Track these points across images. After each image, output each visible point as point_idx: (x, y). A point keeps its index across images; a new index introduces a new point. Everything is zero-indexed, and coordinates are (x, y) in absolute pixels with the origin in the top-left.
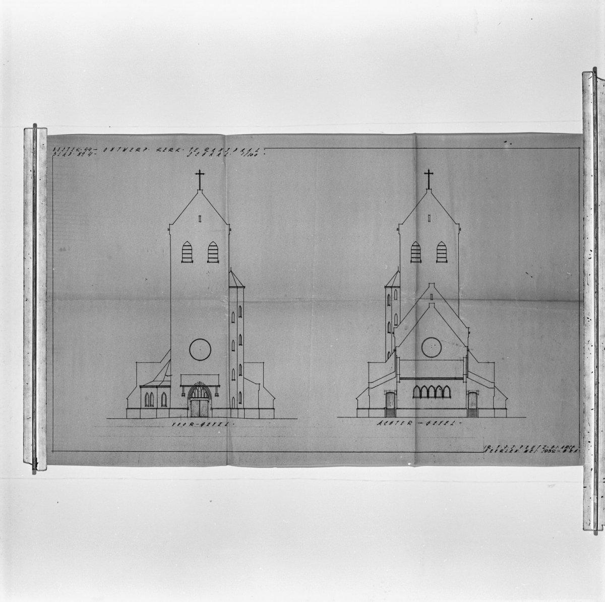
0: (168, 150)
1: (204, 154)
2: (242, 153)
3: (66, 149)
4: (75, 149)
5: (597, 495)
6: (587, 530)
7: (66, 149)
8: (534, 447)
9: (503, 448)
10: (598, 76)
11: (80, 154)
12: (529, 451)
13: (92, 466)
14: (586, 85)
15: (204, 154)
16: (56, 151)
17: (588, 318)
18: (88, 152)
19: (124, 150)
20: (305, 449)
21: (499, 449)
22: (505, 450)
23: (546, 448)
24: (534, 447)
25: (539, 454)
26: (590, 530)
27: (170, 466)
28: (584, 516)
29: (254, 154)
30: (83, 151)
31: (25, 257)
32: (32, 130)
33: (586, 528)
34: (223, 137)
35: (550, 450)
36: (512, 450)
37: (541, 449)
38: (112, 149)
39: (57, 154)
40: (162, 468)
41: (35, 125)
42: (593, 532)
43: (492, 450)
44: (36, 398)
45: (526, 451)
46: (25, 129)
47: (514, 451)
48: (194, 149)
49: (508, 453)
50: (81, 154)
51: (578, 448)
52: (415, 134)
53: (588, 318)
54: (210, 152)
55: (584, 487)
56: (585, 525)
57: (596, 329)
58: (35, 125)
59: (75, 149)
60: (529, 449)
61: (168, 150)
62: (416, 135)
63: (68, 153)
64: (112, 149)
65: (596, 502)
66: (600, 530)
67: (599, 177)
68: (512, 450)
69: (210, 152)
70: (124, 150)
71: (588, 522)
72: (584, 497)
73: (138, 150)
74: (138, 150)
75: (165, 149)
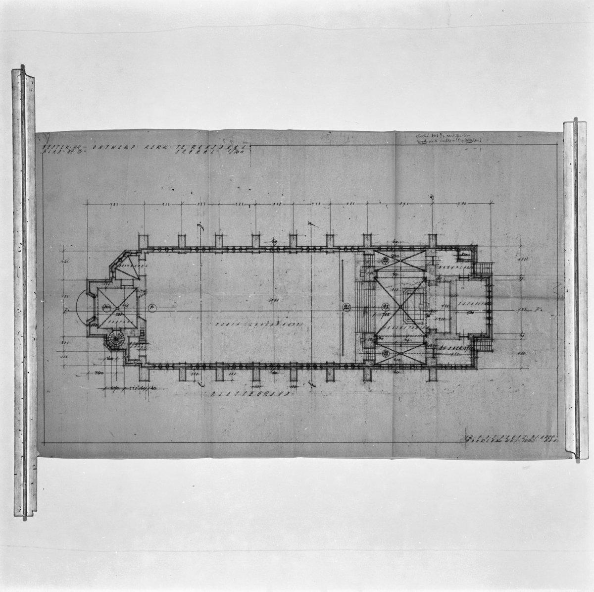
0: (155, 147)
1: (191, 151)
2: (228, 150)
8: (514, 436)
9: (484, 438)
10: (27, 73)
11: (69, 151)
13: (508, 460)
14: (15, 83)
15: (191, 151)
21: (480, 439)
22: (486, 440)
23: (526, 438)
27: (514, 460)
28: (14, 503)
29: (241, 150)
34: (209, 133)
37: (521, 439)
40: (551, 461)
42: (22, 518)
43: (473, 440)
44: (576, 394)
45: (507, 441)
46: (564, 123)
47: (480, 441)
48: (181, 147)
50: (70, 152)
51: (556, 438)
52: (395, 131)
54: (196, 149)
55: (15, 474)
56: (16, 511)
57: (576, 326)
60: (510, 438)
61: (155, 147)
62: (396, 133)
63: (58, 151)
70: (113, 148)
72: (15, 483)
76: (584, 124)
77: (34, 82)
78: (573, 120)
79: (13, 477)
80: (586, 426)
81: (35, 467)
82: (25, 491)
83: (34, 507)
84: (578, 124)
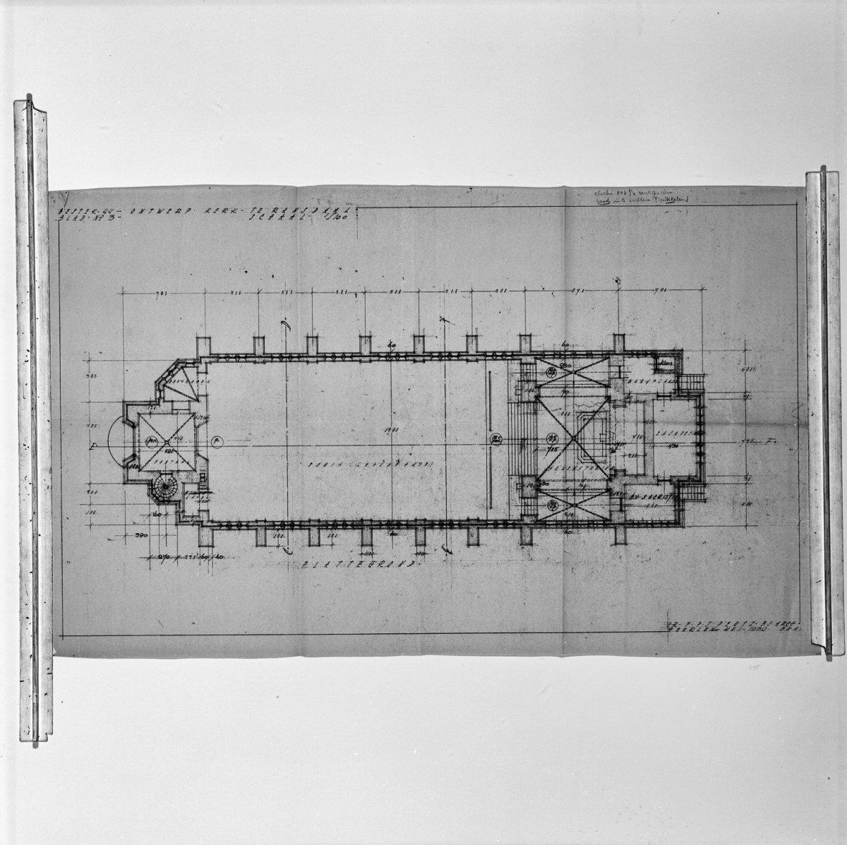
2: (325, 214)
3: (78, 211)
4: (90, 211)
5: (38, 692)
6: (24, 741)
7: (78, 211)
8: (737, 623)
11: (97, 217)
12: (731, 629)
16: (63, 213)
17: (25, 445)
18: (107, 215)
19: (159, 212)
20: (522, 627)
21: (689, 627)
23: (754, 625)
24: (737, 623)
25: (773, 633)
26: (27, 741)
30: (101, 214)
31: (809, 354)
32: (818, 175)
33: (23, 739)
35: (760, 628)
36: (707, 628)
37: (747, 627)
38: (142, 211)
39: (65, 218)
41: (824, 168)
42: (32, 743)
45: (726, 630)
46: (807, 174)
49: (701, 634)
53: (25, 445)
54: (279, 213)
56: (22, 735)
58: (824, 168)
59: (90, 211)
60: (731, 626)
64: (142, 211)
65: (35, 702)
66: (41, 741)
67: (28, 265)
68: (707, 628)
69: (279, 213)
70: (159, 212)
71: (27, 730)
72: (21, 694)
73: (178, 211)
74: (178, 211)
75: (217, 210)
76: (835, 174)
77: (45, 120)
78: (819, 170)
79: (19, 686)
80: (841, 607)
81: (49, 671)
82: (36, 705)
83: (49, 728)
84: (827, 175)
